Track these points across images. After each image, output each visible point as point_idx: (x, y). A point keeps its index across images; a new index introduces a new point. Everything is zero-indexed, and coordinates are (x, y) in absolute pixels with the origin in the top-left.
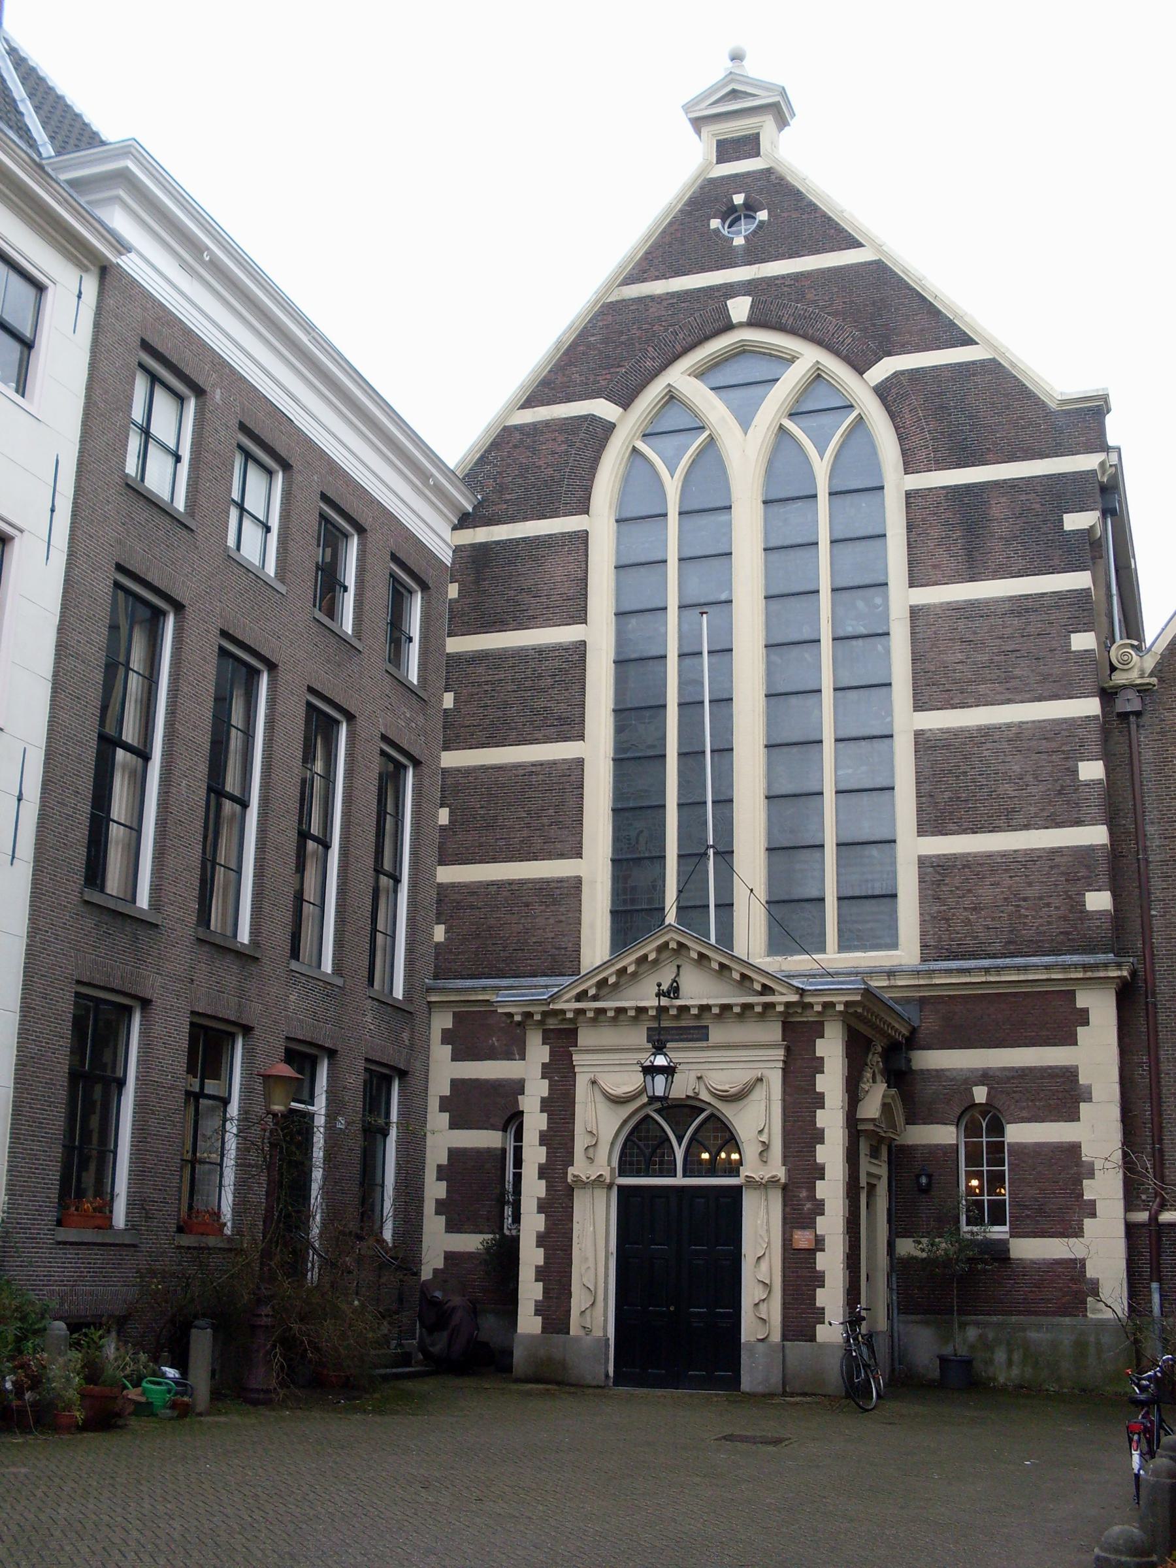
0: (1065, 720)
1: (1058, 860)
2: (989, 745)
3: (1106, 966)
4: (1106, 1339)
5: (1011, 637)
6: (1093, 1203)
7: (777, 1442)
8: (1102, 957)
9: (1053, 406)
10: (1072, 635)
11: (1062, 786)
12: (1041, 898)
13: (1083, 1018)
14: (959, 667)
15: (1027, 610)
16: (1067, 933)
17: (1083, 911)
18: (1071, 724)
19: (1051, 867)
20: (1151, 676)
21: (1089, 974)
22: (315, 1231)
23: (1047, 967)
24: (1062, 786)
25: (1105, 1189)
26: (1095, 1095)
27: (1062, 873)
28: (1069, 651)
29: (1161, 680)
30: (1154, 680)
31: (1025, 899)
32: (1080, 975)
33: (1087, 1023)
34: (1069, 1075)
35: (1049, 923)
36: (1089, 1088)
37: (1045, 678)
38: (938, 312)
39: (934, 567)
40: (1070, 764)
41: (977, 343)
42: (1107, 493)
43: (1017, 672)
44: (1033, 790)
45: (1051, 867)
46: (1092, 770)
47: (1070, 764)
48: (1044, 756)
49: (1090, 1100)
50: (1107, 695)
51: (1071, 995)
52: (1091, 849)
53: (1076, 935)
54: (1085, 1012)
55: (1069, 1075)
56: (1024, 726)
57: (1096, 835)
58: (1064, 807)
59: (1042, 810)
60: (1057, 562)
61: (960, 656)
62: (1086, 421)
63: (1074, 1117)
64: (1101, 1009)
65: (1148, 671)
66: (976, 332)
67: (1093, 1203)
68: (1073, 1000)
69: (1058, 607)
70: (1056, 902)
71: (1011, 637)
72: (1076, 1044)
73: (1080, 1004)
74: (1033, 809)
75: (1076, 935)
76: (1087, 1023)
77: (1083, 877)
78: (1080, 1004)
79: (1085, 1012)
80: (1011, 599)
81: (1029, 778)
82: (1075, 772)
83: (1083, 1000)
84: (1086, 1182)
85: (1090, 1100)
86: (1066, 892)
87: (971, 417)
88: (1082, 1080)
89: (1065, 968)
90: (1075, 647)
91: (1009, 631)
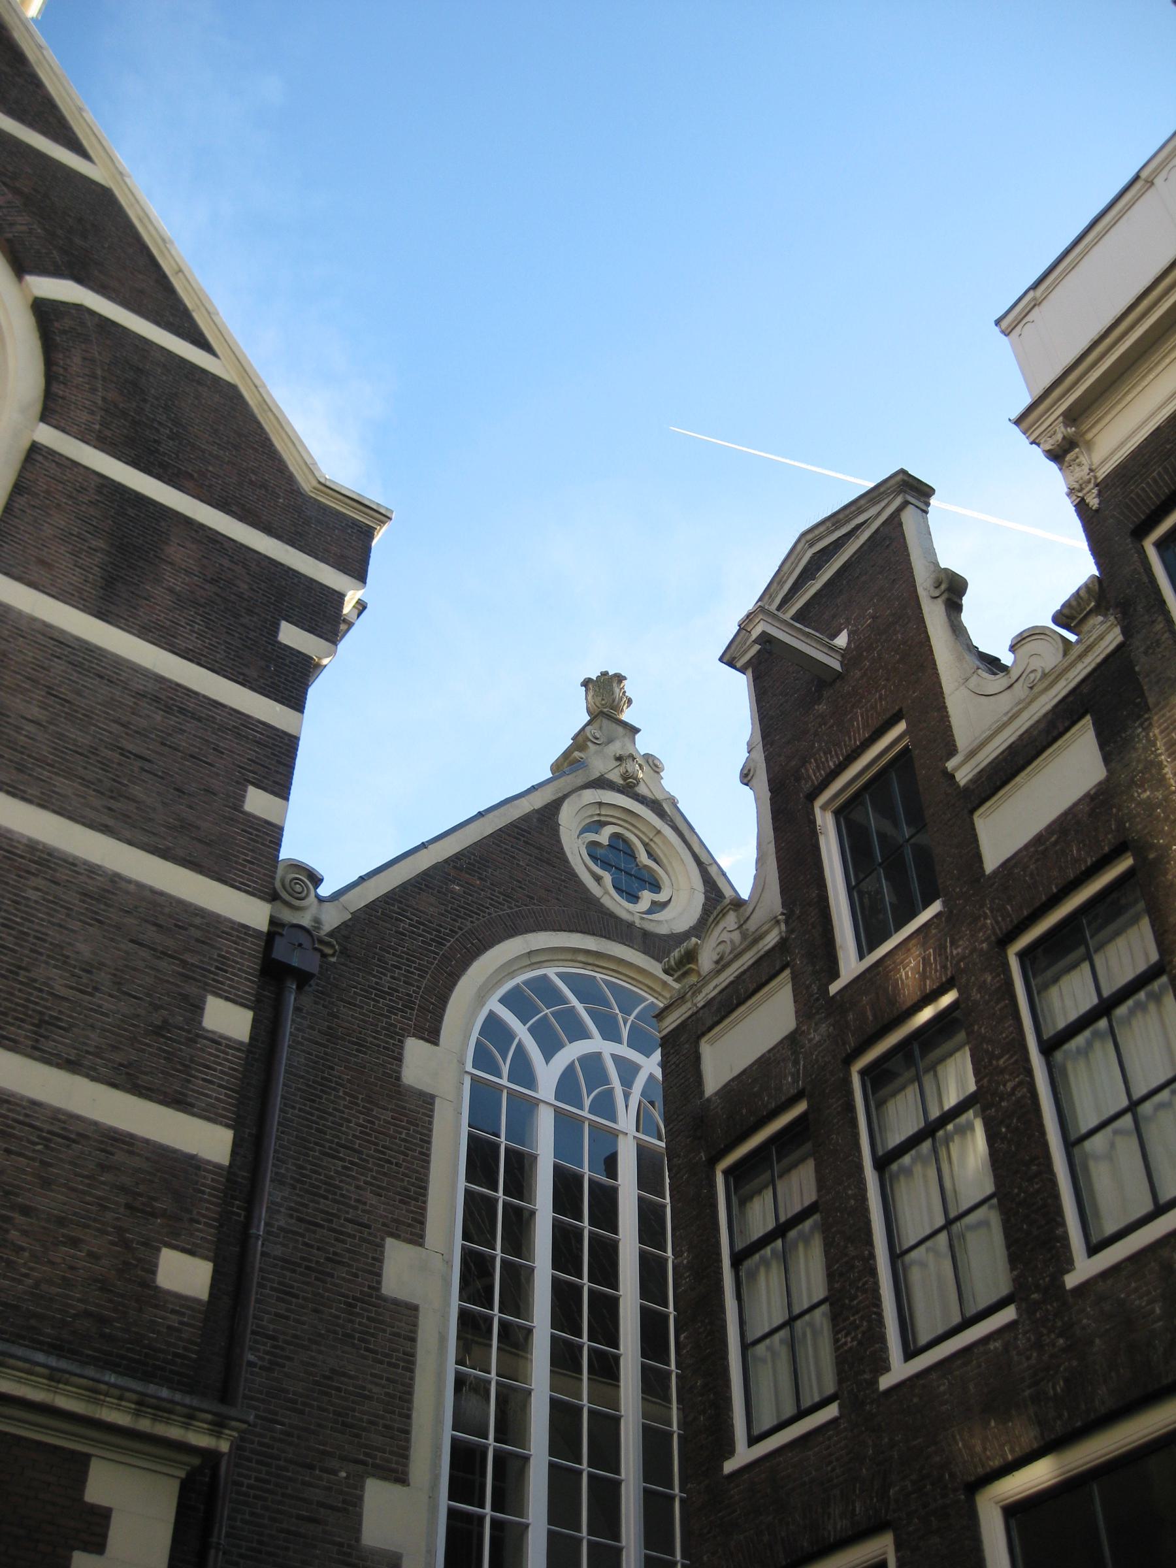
1: (119, 1157)
2: (39, 882)
9: (306, 485)
11: (165, 1021)
12: (61, 1222)
14: (31, 728)
15: (182, 711)
16: (102, 1320)
18: (212, 926)
19: (103, 1167)
21: (144, 1425)
24: (165, 1021)
27: (123, 1189)
31: (26, 1211)
32: (122, 1419)
39: (42, 562)
40: (192, 989)
42: (327, 618)
43: (136, 790)
45: (103, 1167)
48: (144, 953)
51: (78, 1465)
52: (191, 1164)
53: (120, 1338)
54: (102, 1516)
56: (123, 885)
57: (209, 1141)
58: (161, 1063)
59: (115, 1048)
61: (35, 712)
75: (120, 1338)
79: (102, 1516)
80: (160, 679)
82: (198, 1009)
83: (106, 1484)
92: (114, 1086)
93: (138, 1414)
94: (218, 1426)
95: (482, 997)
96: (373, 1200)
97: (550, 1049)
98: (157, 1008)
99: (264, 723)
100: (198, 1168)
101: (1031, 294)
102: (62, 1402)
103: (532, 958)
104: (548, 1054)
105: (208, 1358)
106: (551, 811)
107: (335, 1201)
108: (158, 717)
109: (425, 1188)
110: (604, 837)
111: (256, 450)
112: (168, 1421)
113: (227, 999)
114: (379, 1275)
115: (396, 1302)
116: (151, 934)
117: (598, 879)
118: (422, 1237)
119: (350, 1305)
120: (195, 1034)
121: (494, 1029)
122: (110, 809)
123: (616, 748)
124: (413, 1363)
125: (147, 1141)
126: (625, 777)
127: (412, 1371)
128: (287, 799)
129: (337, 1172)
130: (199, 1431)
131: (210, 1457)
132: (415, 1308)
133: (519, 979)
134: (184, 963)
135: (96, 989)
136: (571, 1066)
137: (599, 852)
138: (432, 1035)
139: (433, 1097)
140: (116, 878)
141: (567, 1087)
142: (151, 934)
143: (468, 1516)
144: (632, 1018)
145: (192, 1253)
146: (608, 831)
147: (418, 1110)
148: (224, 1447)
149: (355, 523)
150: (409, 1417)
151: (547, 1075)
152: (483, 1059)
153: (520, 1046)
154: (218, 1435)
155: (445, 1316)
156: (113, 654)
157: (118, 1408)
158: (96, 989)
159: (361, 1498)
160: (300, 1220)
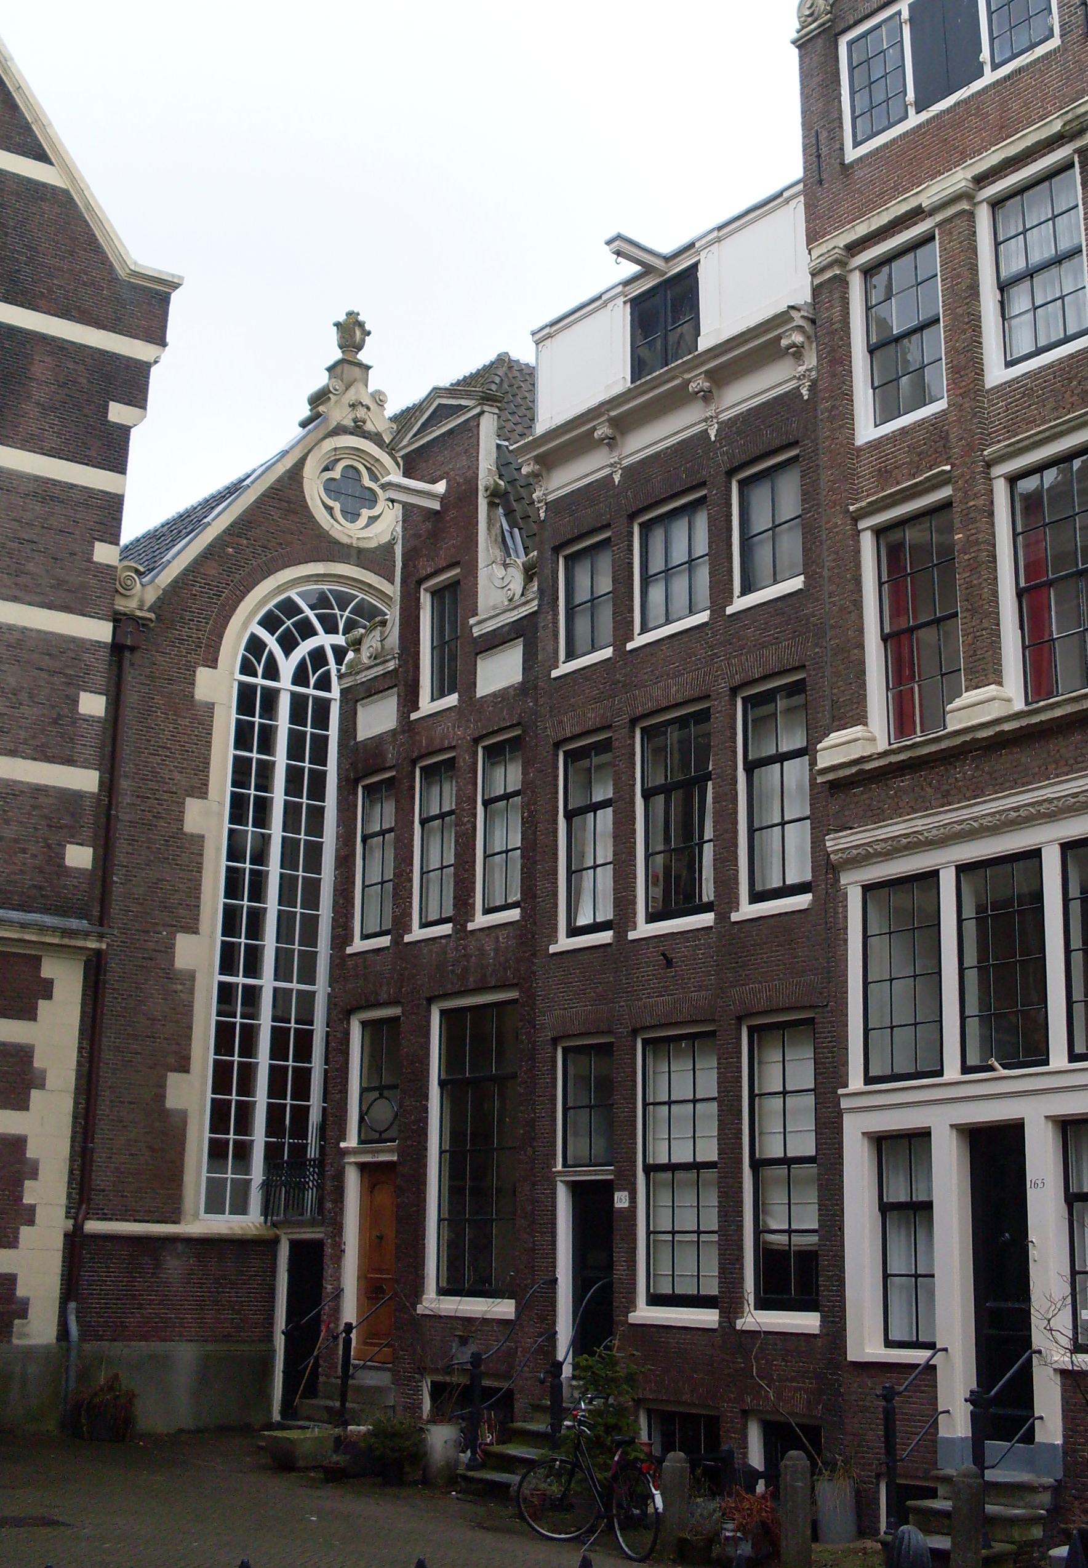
0: (73, 640)
1: (42, 800)
3: (87, 935)
4: (32, 1369)
5: (30, 524)
6: (32, 1209)
7: (48, 1522)
8: (74, 923)
9: (122, 273)
10: (97, 544)
11: (59, 714)
12: (16, 841)
13: (46, 989)
15: (52, 498)
16: (41, 888)
17: (61, 865)
19: (34, 807)
20: (150, 610)
21: (66, 941)
22: (350, 1312)
23: (23, 926)
24: (59, 714)
25: (48, 1192)
26: (50, 1083)
28: (90, 560)
29: (158, 617)
30: (152, 616)
32: (56, 941)
33: (49, 997)
34: (22, 1055)
35: (22, 872)
36: (43, 1072)
37: (60, 584)
38: (15, 107)
40: (71, 691)
41: (51, 164)
43: (30, 567)
44: (25, 710)
45: (34, 807)
46: (92, 705)
47: (71, 691)
49: (42, 1086)
50: (118, 619)
51: (38, 959)
52: (78, 795)
53: (50, 892)
54: (49, 983)
55: (22, 1055)
57: (84, 780)
58: (55, 741)
59: (34, 737)
60: (93, 453)
62: (145, 307)
63: (22, 1105)
64: (67, 982)
65: (147, 605)
66: (53, 145)
67: (32, 1209)
68: (38, 968)
69: (87, 506)
70: (33, 848)
71: (30, 524)
72: (35, 1019)
73: (46, 972)
74: (23, 734)
75: (50, 892)
76: (49, 997)
77: (66, 826)
78: (46, 972)
79: (49, 983)
80: (37, 479)
81: (24, 696)
82: (75, 702)
83: (48, 969)
84: (27, 1183)
85: (42, 1086)
86: (46, 840)
87: (30, 248)
88: (37, 1064)
89: (42, 929)
90: (97, 558)
91: (28, 516)
92: (35, 759)
93: (62, 937)
94: (101, 937)
95: (246, 624)
96: (177, 776)
97: (288, 650)
98: (53, 707)
99: (102, 491)
100: (82, 797)
101: (715, 234)
102: (27, 937)
103: (280, 589)
104: (287, 652)
105: (97, 897)
106: (295, 474)
107: (157, 781)
108: (38, 507)
109: (208, 763)
110: (336, 474)
111: (85, 250)
112: (76, 939)
113: (91, 692)
114: (182, 821)
115: (192, 835)
116: (47, 662)
117: (330, 509)
118: (206, 793)
119: (167, 841)
120: (76, 718)
121: (255, 646)
122: (16, 584)
123: (351, 396)
124: (201, 868)
125: (54, 787)
126: (355, 421)
127: (200, 872)
128: (124, 473)
129: (158, 764)
130: (92, 941)
131: (98, 953)
132: (203, 837)
133: (270, 606)
134: (66, 675)
135: (21, 704)
136: (303, 660)
137: (333, 486)
138: (213, 663)
139: (213, 704)
140: (24, 630)
141: (300, 677)
142: (47, 662)
143: (236, 869)
144: (347, 613)
145: (81, 845)
146: (340, 466)
147: (192, 848)
148: (104, 946)
149: (157, 292)
150: (199, 898)
151: (287, 666)
152: (247, 668)
153: (271, 653)
154: (101, 942)
155: (220, 836)
156: (8, 469)
157: (53, 936)
158: (21, 704)
159: (174, 945)
160: (138, 797)
